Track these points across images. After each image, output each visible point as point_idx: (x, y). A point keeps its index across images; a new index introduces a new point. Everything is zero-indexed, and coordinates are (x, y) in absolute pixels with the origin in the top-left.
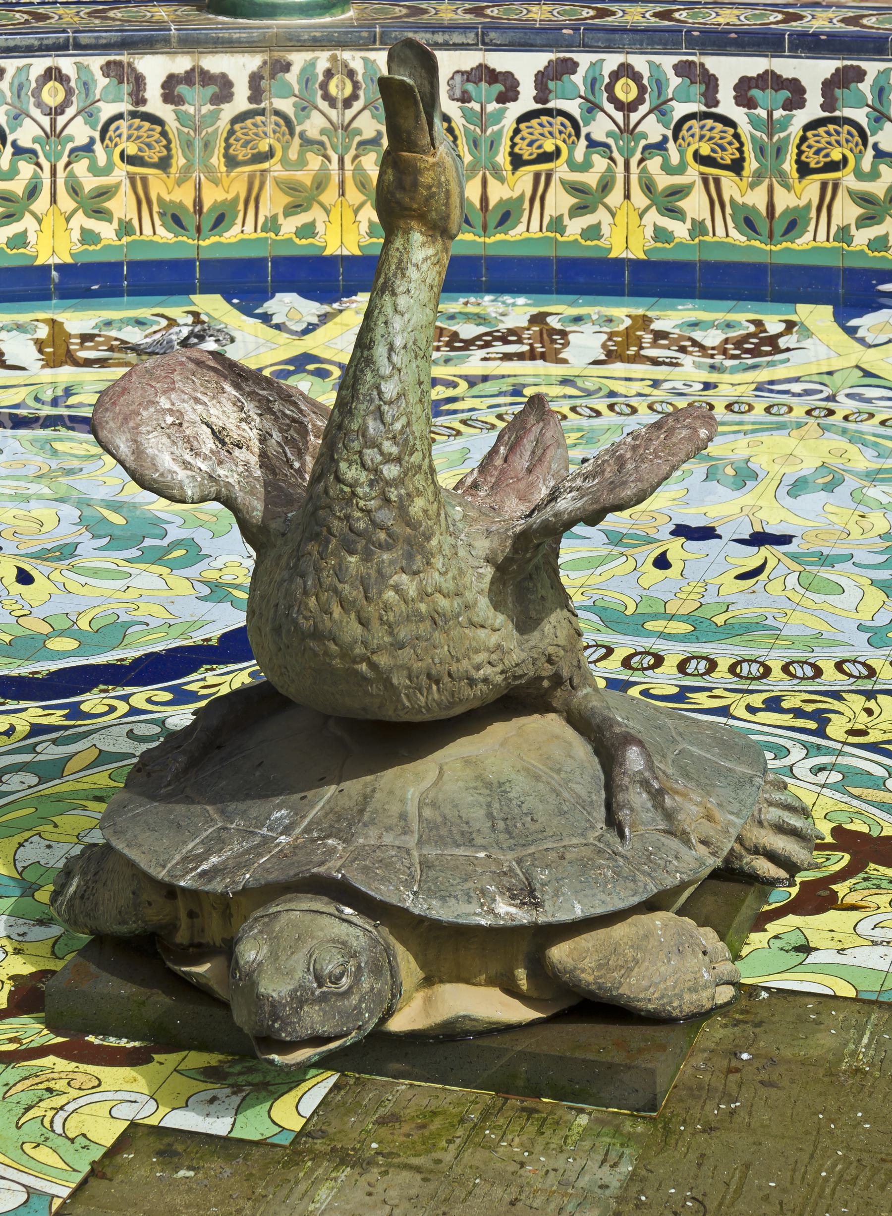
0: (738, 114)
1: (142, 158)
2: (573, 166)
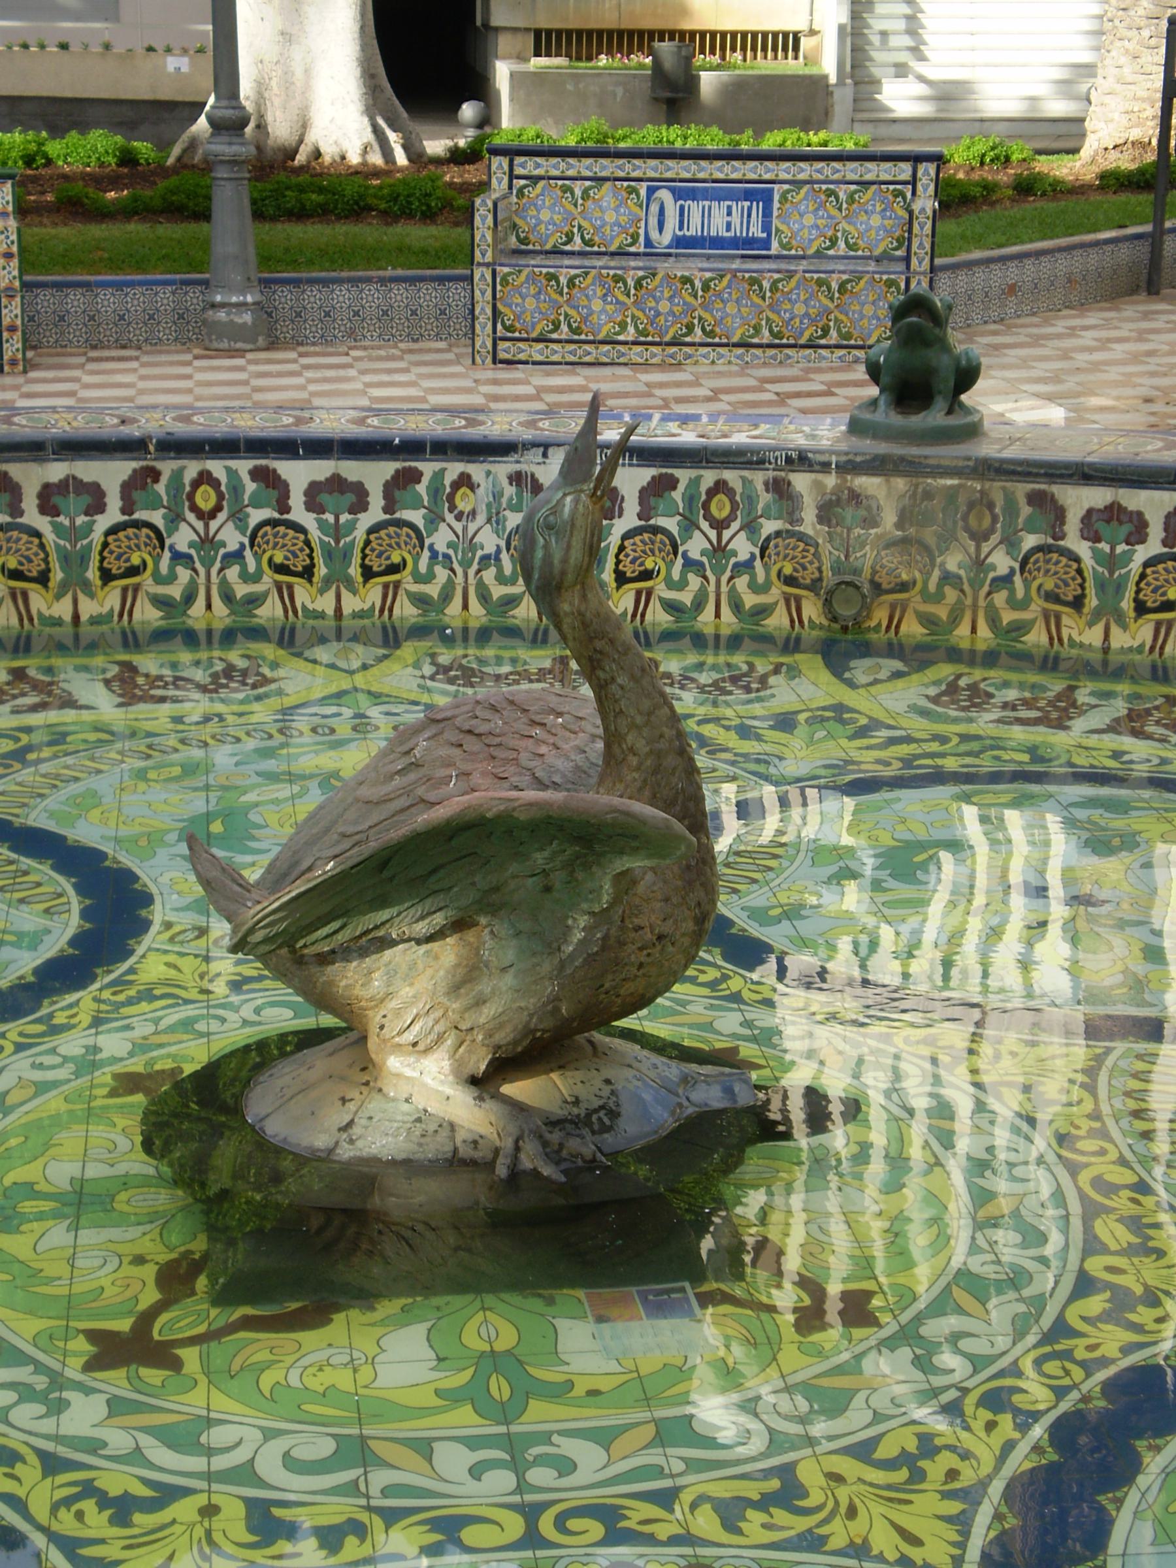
0: (308, 520)
1: (796, 579)
2: (158, 579)
